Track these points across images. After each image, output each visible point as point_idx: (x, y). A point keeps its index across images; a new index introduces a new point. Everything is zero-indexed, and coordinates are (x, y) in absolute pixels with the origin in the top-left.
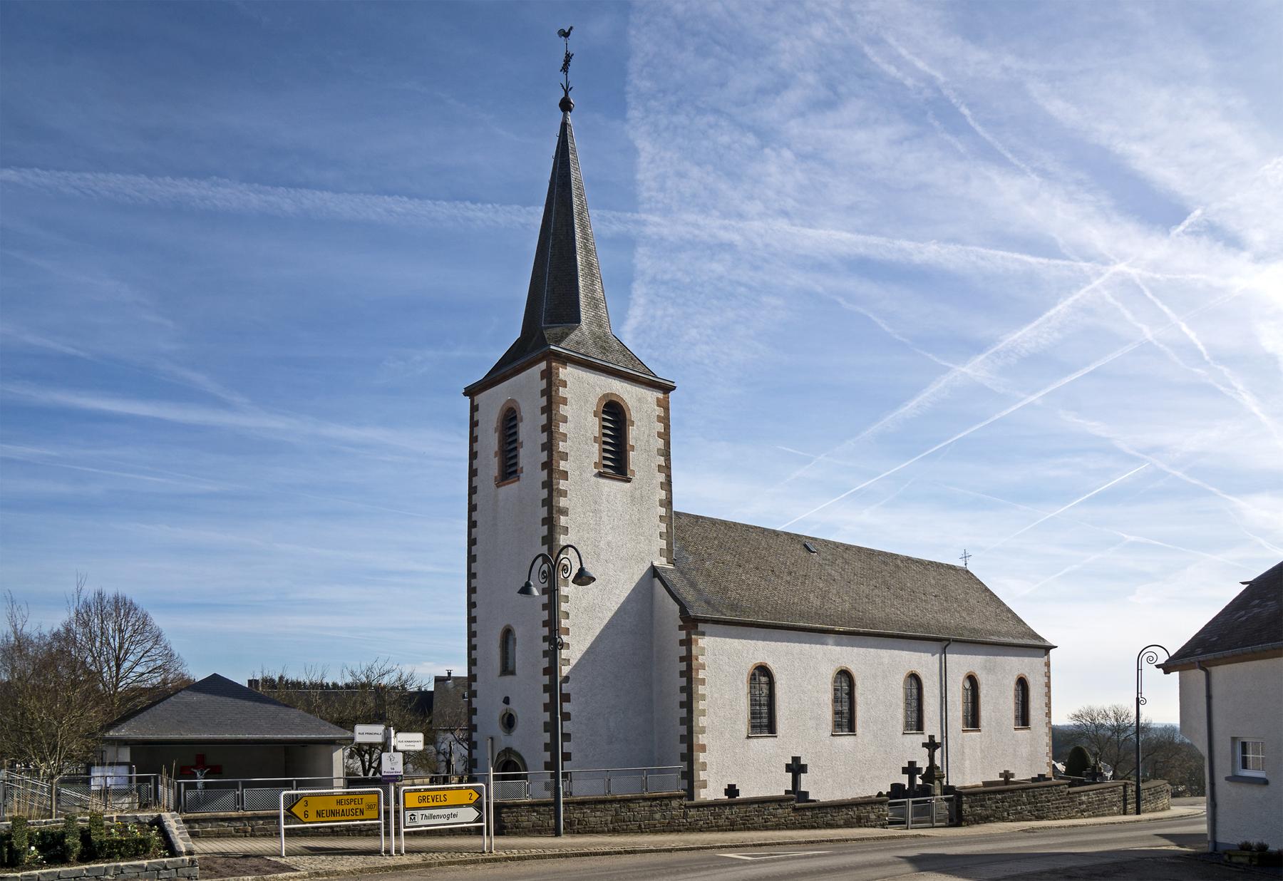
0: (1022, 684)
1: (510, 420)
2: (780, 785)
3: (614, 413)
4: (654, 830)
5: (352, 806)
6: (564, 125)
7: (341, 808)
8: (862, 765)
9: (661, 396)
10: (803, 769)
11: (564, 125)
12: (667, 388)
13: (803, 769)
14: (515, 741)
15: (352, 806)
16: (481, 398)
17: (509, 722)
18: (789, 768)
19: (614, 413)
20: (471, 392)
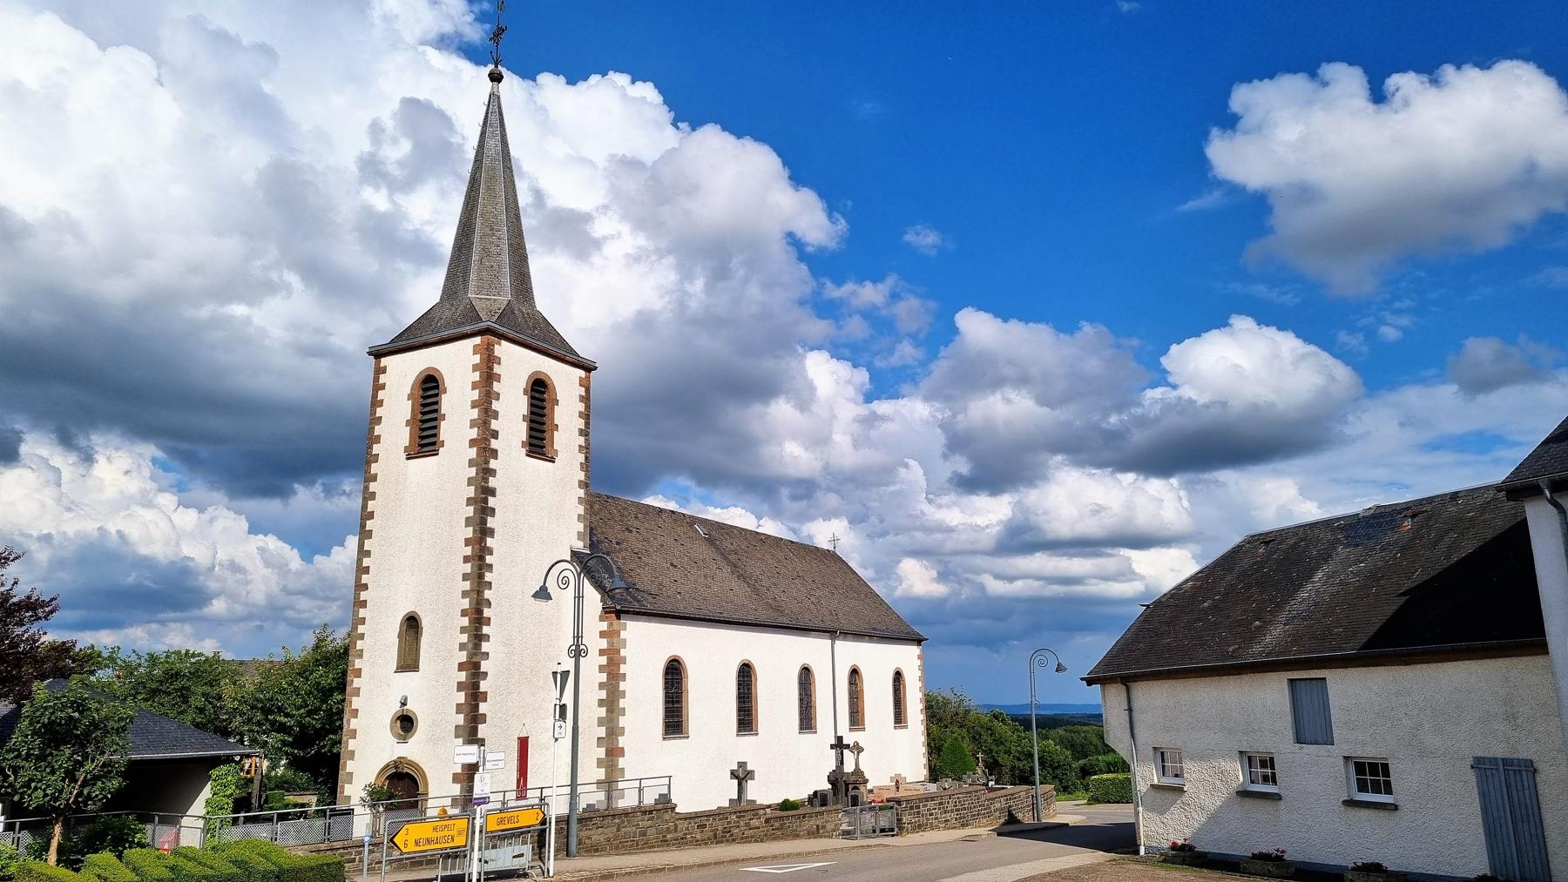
0: (806, 674)
1: (430, 385)
2: (721, 794)
3: (539, 389)
4: (648, 846)
5: (446, 833)
6: (494, 99)
7: (435, 835)
8: (792, 768)
9: (582, 373)
10: (749, 775)
11: (494, 99)
12: (588, 368)
13: (749, 775)
14: (414, 750)
15: (446, 833)
16: (384, 361)
17: (406, 723)
18: (734, 774)
19: (539, 389)
20: (378, 354)
